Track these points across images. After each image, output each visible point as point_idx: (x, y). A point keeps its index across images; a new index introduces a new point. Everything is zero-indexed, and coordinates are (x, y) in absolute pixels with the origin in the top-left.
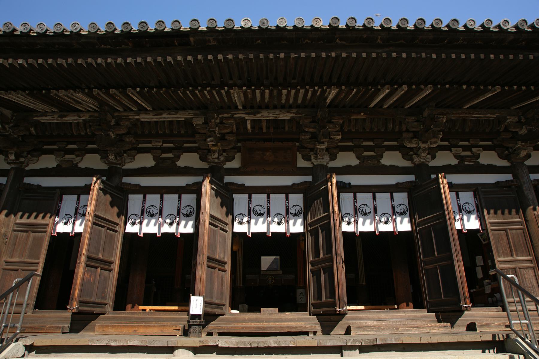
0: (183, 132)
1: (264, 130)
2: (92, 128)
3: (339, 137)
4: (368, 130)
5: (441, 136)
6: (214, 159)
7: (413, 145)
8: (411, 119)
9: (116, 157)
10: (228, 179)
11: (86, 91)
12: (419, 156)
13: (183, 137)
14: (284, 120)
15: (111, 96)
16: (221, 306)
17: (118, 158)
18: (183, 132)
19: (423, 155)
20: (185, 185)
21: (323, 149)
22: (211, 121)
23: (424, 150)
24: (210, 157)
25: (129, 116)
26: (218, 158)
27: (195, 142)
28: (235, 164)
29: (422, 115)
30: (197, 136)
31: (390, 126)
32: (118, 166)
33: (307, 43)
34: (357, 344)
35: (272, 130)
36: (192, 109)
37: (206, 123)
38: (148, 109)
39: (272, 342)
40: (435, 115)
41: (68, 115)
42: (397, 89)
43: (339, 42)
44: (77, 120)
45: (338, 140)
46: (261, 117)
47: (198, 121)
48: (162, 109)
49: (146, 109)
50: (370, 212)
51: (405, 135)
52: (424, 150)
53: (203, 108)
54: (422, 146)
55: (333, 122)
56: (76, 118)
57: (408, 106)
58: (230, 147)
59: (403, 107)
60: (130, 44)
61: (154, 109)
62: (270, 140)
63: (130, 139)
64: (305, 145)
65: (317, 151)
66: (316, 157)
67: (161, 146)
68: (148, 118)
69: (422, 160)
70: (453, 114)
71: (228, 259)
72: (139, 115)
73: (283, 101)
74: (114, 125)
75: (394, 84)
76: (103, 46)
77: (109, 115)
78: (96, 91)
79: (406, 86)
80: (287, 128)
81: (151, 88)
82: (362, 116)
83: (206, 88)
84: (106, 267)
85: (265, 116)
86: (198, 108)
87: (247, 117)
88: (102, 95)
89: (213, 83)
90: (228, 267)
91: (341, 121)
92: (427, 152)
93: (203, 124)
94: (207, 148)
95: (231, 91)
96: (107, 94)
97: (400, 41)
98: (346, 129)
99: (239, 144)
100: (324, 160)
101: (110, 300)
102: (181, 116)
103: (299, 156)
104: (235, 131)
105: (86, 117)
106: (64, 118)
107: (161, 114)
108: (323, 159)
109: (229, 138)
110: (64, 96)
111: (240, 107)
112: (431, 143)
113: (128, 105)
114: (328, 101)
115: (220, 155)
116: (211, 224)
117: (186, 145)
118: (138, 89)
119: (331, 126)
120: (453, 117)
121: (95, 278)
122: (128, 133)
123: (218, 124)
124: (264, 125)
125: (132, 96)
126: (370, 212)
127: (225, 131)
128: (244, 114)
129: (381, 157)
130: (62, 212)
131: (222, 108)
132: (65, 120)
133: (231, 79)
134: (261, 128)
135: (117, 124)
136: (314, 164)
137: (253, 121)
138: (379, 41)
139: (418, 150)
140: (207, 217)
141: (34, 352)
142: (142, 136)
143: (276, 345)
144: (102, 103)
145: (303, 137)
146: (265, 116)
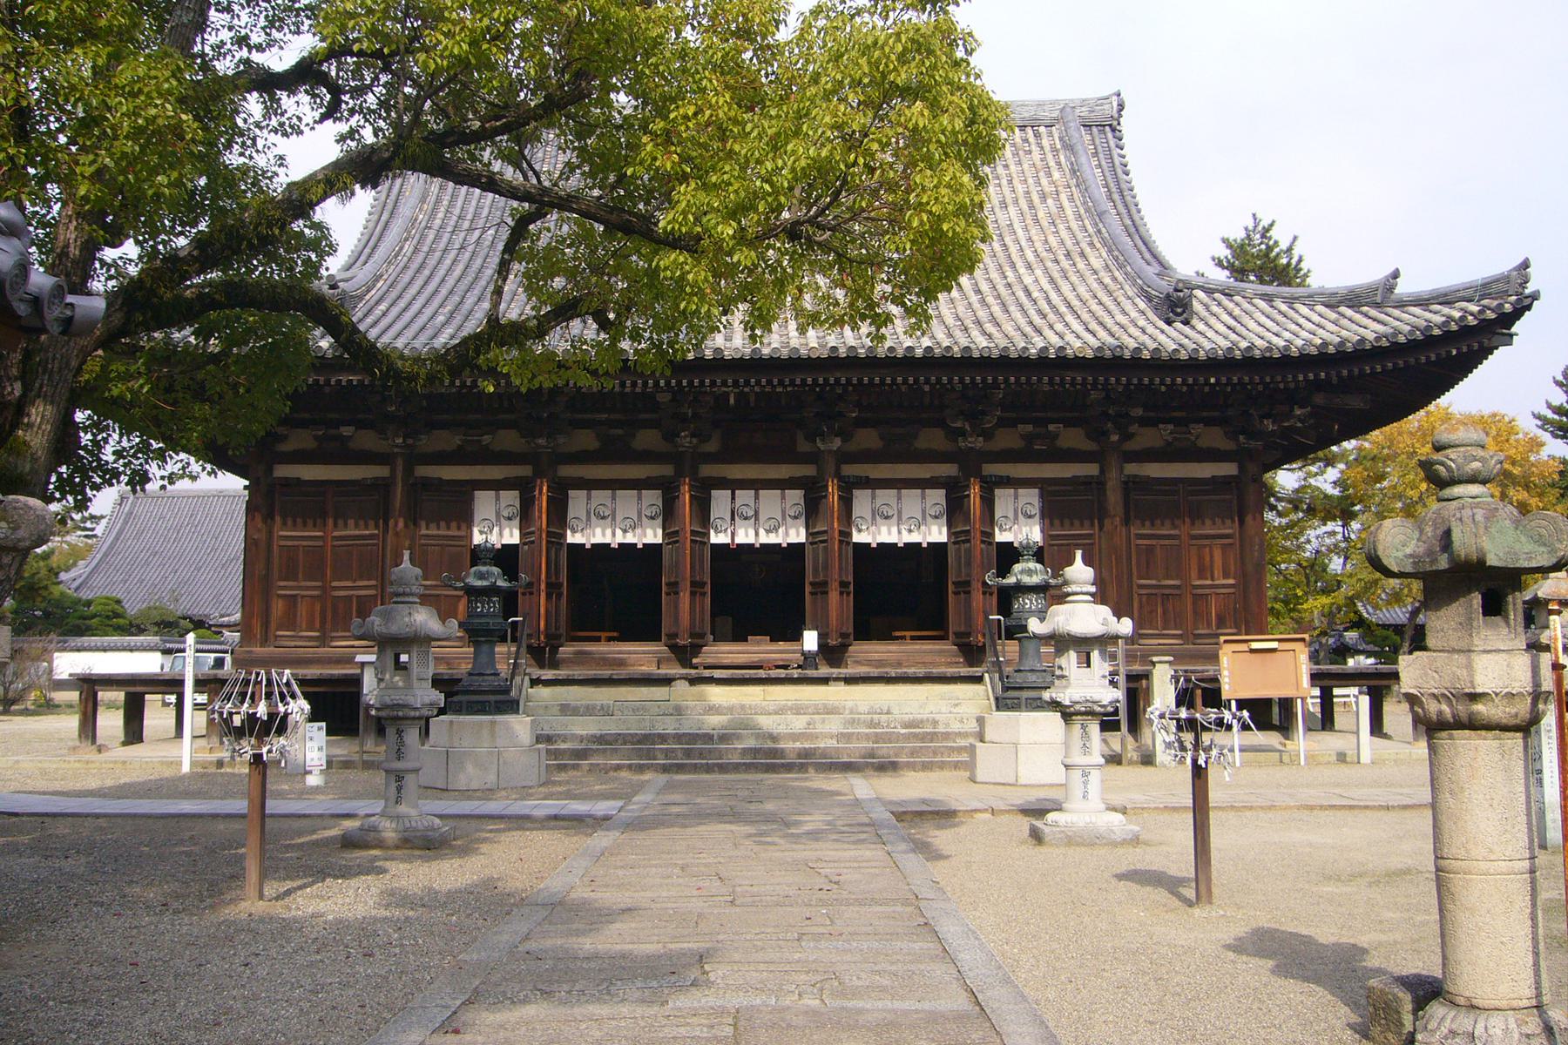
28: (712, 446)
90: (708, 588)
103: (800, 437)
130: (477, 517)
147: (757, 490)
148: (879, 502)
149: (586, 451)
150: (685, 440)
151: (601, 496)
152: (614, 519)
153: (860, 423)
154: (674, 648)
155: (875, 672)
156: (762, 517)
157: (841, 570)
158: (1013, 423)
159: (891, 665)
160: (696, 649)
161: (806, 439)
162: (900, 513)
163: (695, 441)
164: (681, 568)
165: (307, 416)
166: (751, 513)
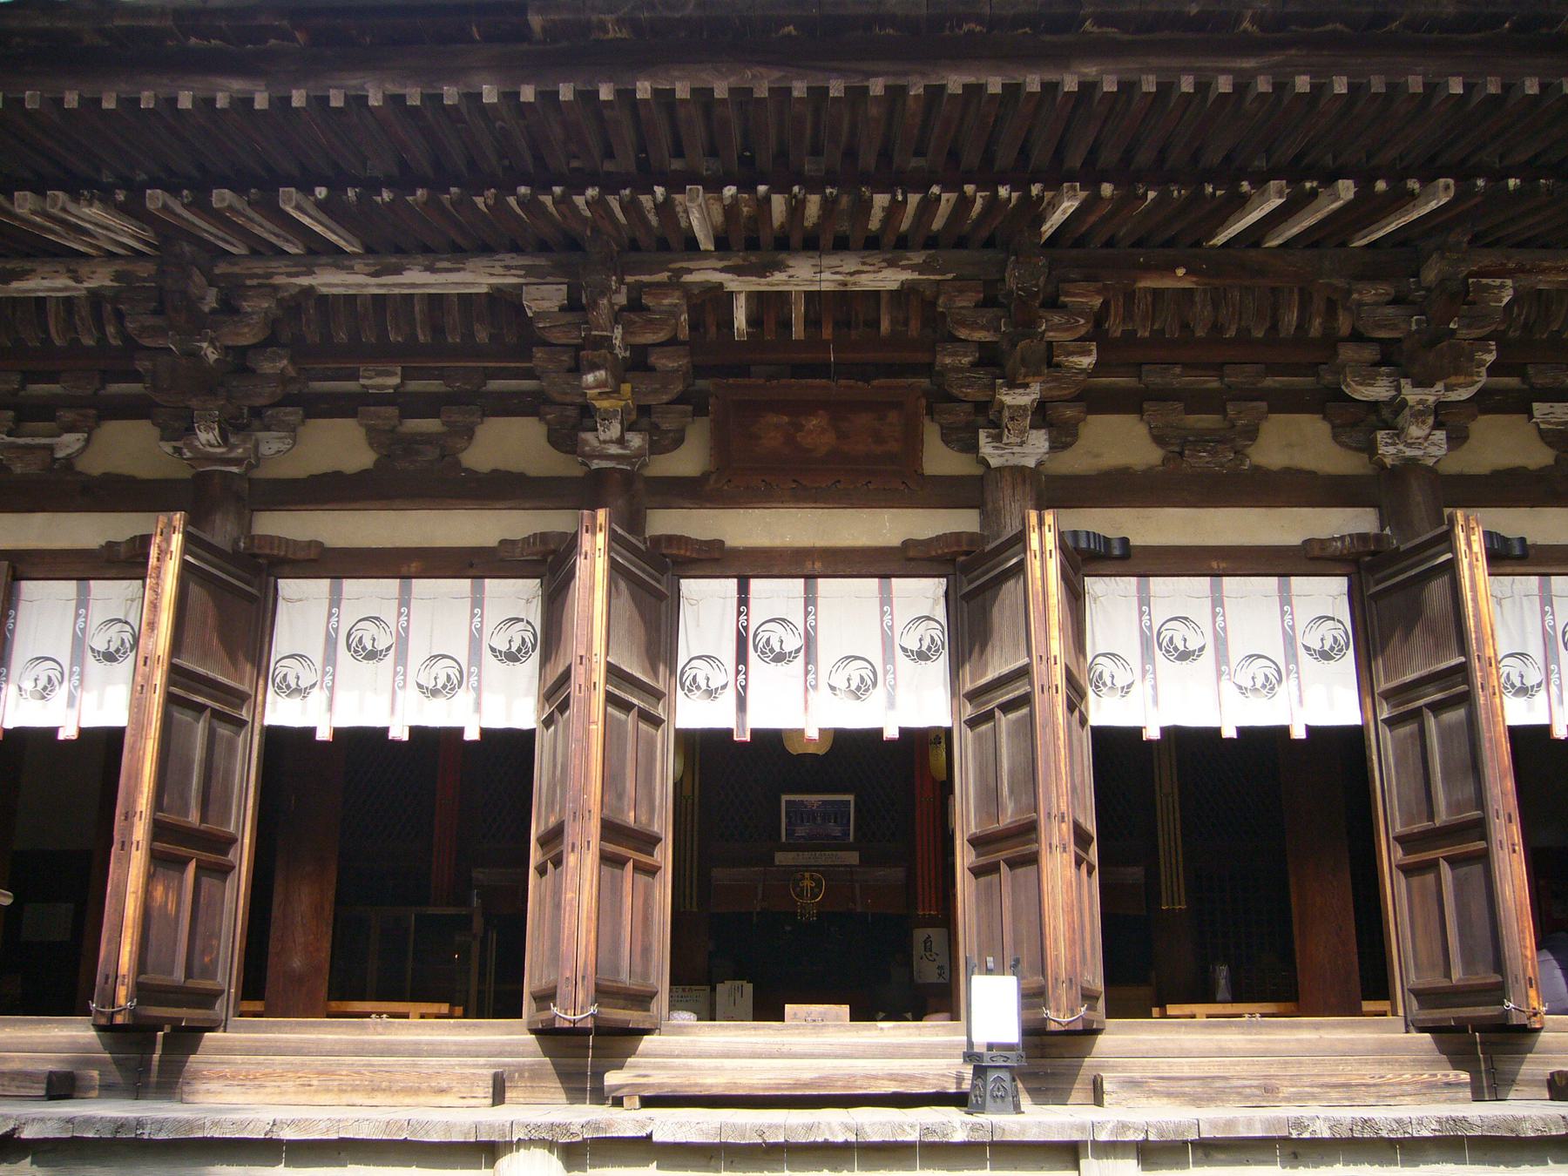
0: (482, 336)
1: (798, 331)
2: (130, 325)
3: (1087, 361)
4: (1200, 333)
5: (1490, 358)
6: (605, 442)
7: (1379, 391)
8: (1370, 293)
9: (224, 436)
10: (666, 522)
11: (121, 196)
12: (1398, 433)
13: (484, 355)
14: (876, 295)
15: (217, 217)
16: (642, 999)
17: (232, 440)
18: (482, 336)
19: (1415, 431)
20: (495, 544)
21: (1023, 408)
22: (594, 304)
23: (1421, 413)
24: (589, 436)
25: (270, 276)
26: (621, 441)
27: (529, 374)
28: (687, 461)
29: (1416, 275)
30: (539, 353)
31: (1291, 318)
32: (235, 469)
33: (971, 33)
34: (1131, 1136)
35: (827, 333)
36: (516, 249)
37: (573, 305)
38: (349, 249)
39: (833, 1125)
40: (1470, 275)
41: (33, 271)
42: (1314, 194)
43: (1095, 29)
44: (66, 289)
45: (1083, 371)
46: (786, 283)
47: (545, 298)
48: (399, 250)
49: (340, 251)
50: (1202, 649)
51: (1347, 352)
52: (1419, 416)
53: (563, 248)
54: (1412, 395)
55: (1064, 306)
56: (63, 281)
57: (1364, 242)
58: (665, 398)
59: (1343, 244)
60: (298, 35)
61: (369, 250)
62: (819, 370)
63: (275, 365)
64: (955, 391)
65: (1000, 412)
66: (998, 438)
67: (396, 388)
68: (347, 286)
69: (1409, 452)
70: (1543, 271)
71: (663, 825)
72: (310, 273)
73: (874, 224)
74: (213, 311)
75: (1304, 173)
76: (193, 40)
77: (198, 278)
78: (155, 199)
79: (1350, 183)
80: (885, 326)
81: (374, 186)
82: (1180, 278)
83: (586, 188)
84: (213, 857)
85: (803, 276)
86: (543, 247)
87: (732, 283)
88: (179, 210)
89: (609, 166)
90: (664, 856)
91: (1097, 302)
92: (1431, 421)
93: (562, 309)
94: (580, 400)
95: (678, 197)
96: (201, 205)
97: (1330, 27)
98: (1115, 327)
99: (701, 384)
100: (1026, 449)
101: (227, 974)
102: (476, 278)
104: (684, 333)
105: (100, 278)
106: (15, 285)
107: (398, 271)
108: (1022, 444)
109: (666, 362)
110: (34, 212)
111: (706, 244)
112: (1448, 388)
113: (273, 239)
114: (1048, 228)
115: (629, 427)
116: (611, 699)
117: (494, 385)
118: (321, 192)
119: (1056, 319)
120: (1543, 283)
121: (178, 905)
122: (270, 342)
123: (622, 309)
124: (798, 312)
125: (295, 214)
126: (1202, 649)
127: (650, 338)
128: (722, 270)
129: (1252, 434)
130: (22, 649)
131: (634, 246)
132: (17, 290)
133: (679, 152)
134: (787, 325)
135: (229, 307)
136: (988, 465)
137: (759, 301)
138: (1246, 25)
139: (1397, 413)
140: (599, 675)
141: (29, 1159)
142: (322, 352)
143: (852, 1138)
144: (166, 233)
145: (948, 361)
146: (803, 276)
147: (810, 577)
148: (348, 615)
149: (338, 475)
150: (608, 439)
151: (1178, 595)
152: (402, 659)
153: (1100, 401)
154: (547, 1033)
155: (1252, 1121)
156: (827, 653)
157: (1067, 795)
158: (1519, 404)
159: (1241, 1095)
160: (616, 1040)
161: (946, 440)
162: (1221, 642)
163: (636, 440)
164: (576, 786)
165: (434, 386)
166: (793, 642)
